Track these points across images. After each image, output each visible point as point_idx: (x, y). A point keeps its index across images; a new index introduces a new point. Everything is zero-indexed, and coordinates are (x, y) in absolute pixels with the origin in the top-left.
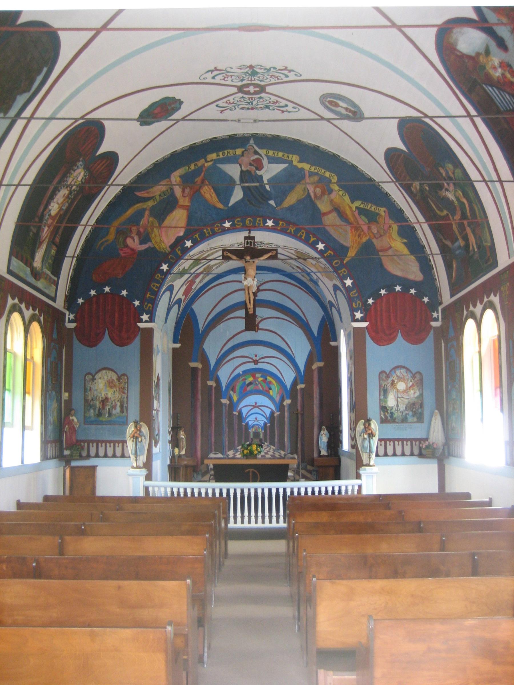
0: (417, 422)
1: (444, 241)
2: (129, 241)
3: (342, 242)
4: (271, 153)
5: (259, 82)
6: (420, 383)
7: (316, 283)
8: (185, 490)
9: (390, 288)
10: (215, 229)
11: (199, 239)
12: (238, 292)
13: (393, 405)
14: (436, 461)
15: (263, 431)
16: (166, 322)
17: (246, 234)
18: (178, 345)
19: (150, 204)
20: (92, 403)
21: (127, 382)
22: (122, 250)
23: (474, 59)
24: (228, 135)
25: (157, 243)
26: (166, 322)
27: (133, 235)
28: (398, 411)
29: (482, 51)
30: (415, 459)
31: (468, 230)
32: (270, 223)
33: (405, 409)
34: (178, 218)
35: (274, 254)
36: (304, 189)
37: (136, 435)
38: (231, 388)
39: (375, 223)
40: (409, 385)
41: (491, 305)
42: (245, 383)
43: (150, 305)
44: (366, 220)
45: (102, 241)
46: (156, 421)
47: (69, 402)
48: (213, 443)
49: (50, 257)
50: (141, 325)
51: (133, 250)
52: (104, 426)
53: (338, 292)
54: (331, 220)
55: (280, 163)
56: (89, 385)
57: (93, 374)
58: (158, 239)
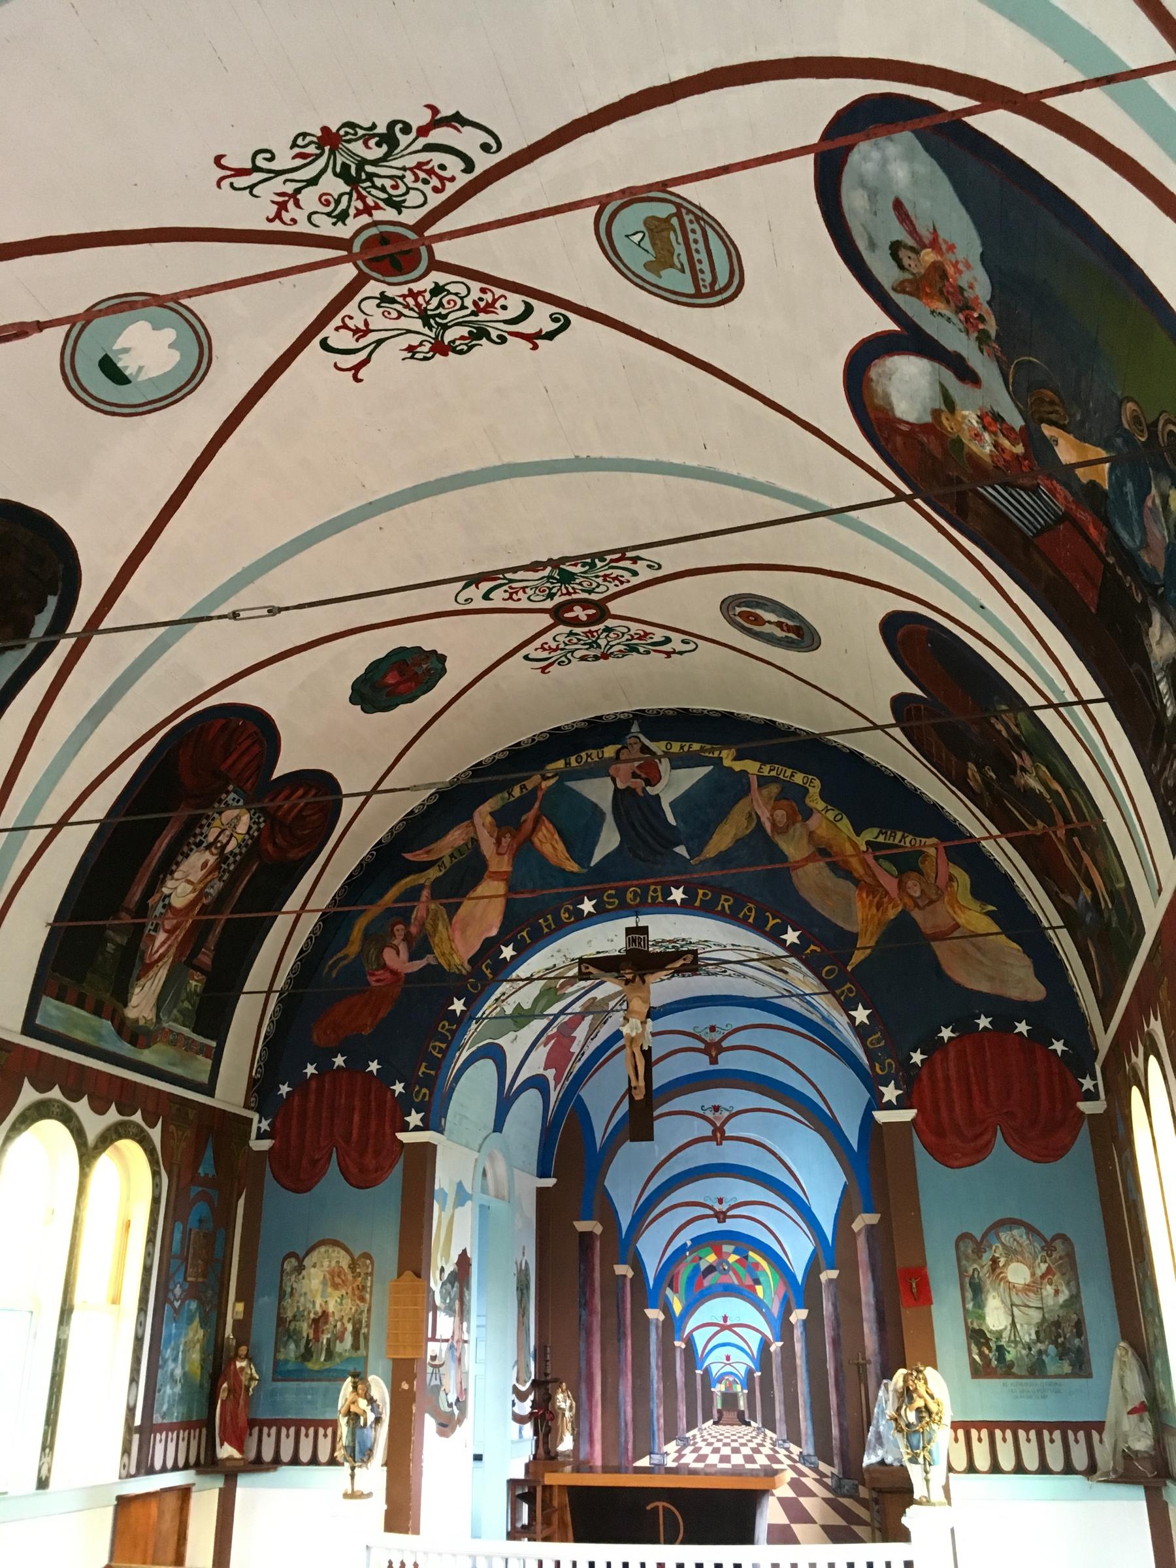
0: (1073, 1375)
2: (389, 955)
3: (840, 923)
4: (676, 747)
5: (585, 596)
9: (965, 1026)
11: (529, 941)
12: (679, 1055)
13: (1002, 1327)
14: (1140, 1492)
15: (746, 1391)
16: (498, 1127)
17: (630, 922)
18: (550, 1182)
19: (433, 874)
21: (371, 1274)
22: (374, 975)
23: (933, 429)
25: (443, 954)
26: (498, 1127)
28: (1016, 1342)
29: (939, 404)
30: (1076, 1482)
33: (1034, 1337)
34: (484, 911)
36: (750, 815)
39: (915, 874)
40: (1039, 1273)
42: (697, 1267)
43: (424, 1090)
45: (335, 958)
49: (184, 996)
50: (404, 1137)
51: (394, 973)
52: (314, 1384)
54: (812, 880)
56: (290, 1282)
57: (301, 1256)
58: (446, 948)
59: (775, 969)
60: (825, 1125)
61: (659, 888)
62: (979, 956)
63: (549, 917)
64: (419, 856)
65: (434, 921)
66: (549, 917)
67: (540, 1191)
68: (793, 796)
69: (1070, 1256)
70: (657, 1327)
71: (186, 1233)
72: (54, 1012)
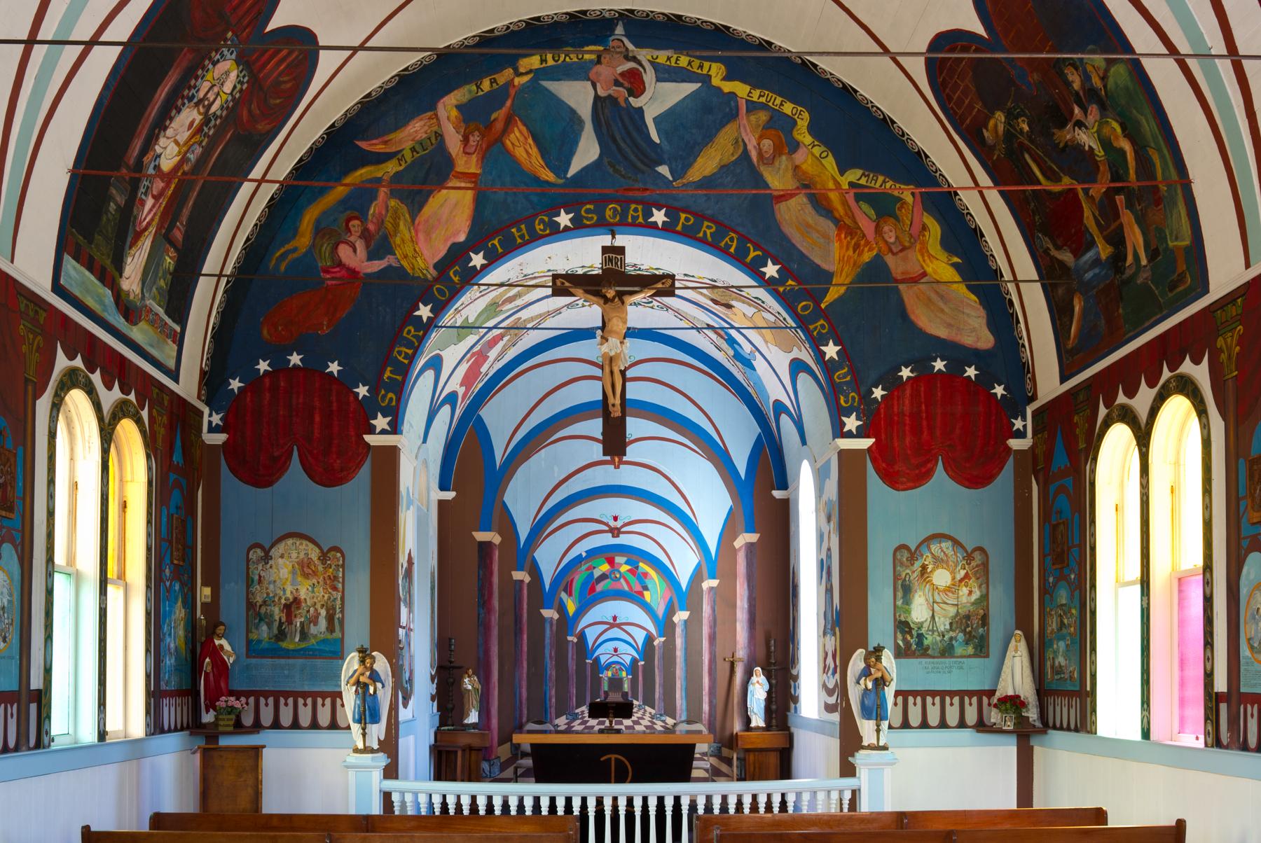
0: (975, 656)
1: (1054, 252)
2: (344, 252)
3: (818, 261)
4: (662, 56)
6: (983, 574)
7: (747, 363)
8: (474, 798)
9: (921, 364)
10: (537, 227)
16: (425, 441)
17: (606, 240)
18: (450, 495)
20: (263, 610)
21: (343, 566)
24: (566, 13)
25: (406, 257)
26: (425, 441)
27: (352, 239)
28: (933, 631)
30: (967, 734)
31: (1127, 218)
32: (659, 217)
34: (452, 211)
35: (667, 285)
36: (737, 142)
37: (362, 679)
38: (562, 587)
39: (892, 220)
40: (958, 577)
41: (1187, 387)
43: (390, 395)
44: (872, 213)
45: (282, 250)
46: (405, 652)
47: (212, 608)
48: (524, 701)
51: (353, 273)
52: (291, 661)
53: (803, 378)
54: (794, 215)
55: (683, 81)
58: (409, 250)
59: (715, 302)
60: (718, 456)
61: (640, 207)
62: (941, 304)
63: (523, 226)
64: (377, 146)
65: (395, 219)
66: (523, 226)
67: (442, 503)
68: (780, 127)
69: (985, 565)
70: (551, 625)
71: (170, 517)
72: (72, 273)
